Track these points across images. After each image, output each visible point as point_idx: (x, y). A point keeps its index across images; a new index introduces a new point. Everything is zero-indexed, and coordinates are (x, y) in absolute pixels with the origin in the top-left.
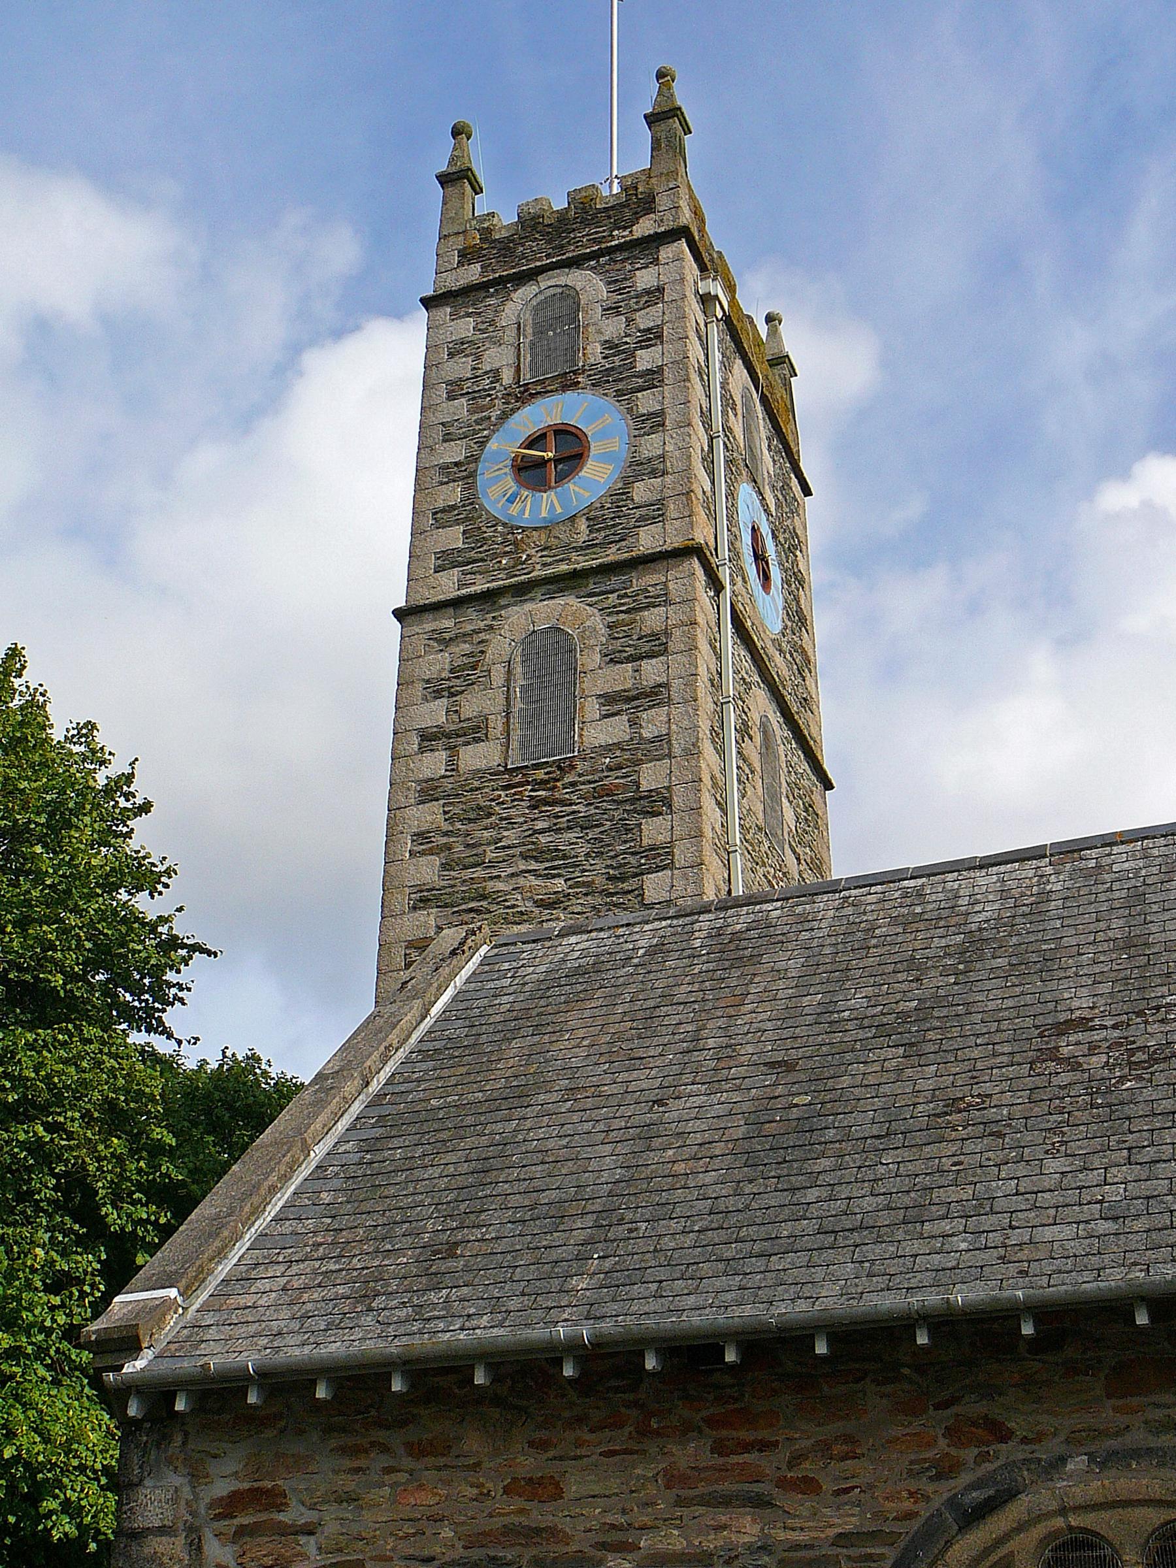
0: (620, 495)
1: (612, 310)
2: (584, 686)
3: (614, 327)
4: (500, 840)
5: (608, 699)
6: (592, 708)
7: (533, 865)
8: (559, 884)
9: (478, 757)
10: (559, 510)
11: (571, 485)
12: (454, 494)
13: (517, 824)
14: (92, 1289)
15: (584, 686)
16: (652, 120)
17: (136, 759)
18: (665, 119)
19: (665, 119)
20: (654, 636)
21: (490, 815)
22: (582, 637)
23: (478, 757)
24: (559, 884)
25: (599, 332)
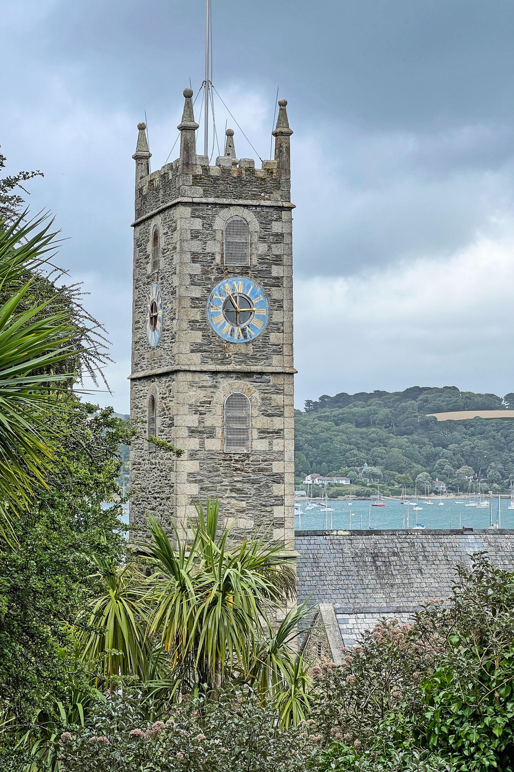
1: (262, 239)
5: (262, 431)
8: (244, 504)
9: (214, 445)
12: (277, 316)
23: (214, 445)
24: (244, 504)
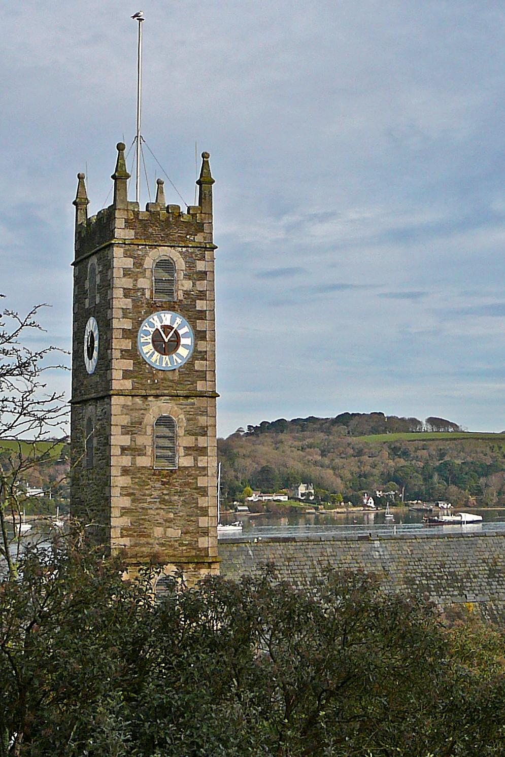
0: (190, 363)
2: (179, 442)
3: (188, 285)
4: (151, 495)
5: (186, 448)
6: (182, 452)
7: (163, 507)
8: (172, 515)
10: (170, 365)
11: (174, 355)
13: (155, 489)
14: (429, 592)
15: (179, 442)
16: (199, 182)
17: (205, 156)
18: (205, 182)
19: (205, 182)
20: (202, 427)
21: (149, 485)
22: (178, 420)
25: (182, 285)
